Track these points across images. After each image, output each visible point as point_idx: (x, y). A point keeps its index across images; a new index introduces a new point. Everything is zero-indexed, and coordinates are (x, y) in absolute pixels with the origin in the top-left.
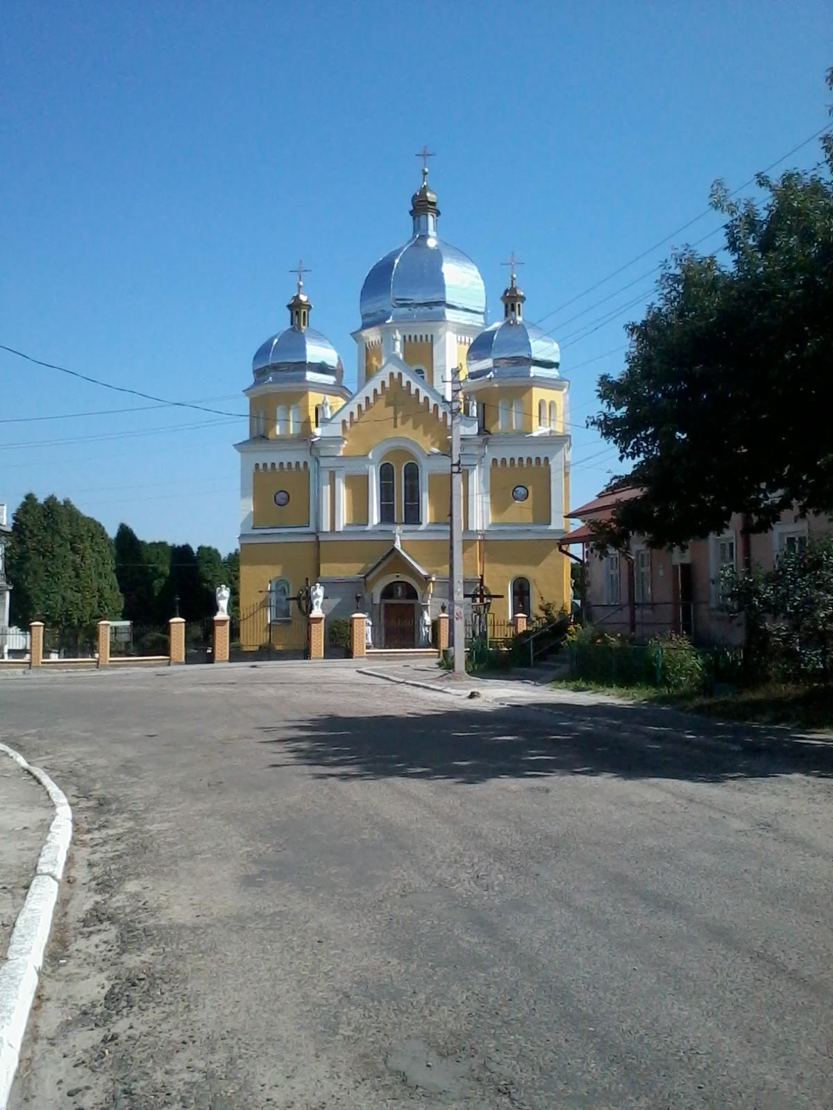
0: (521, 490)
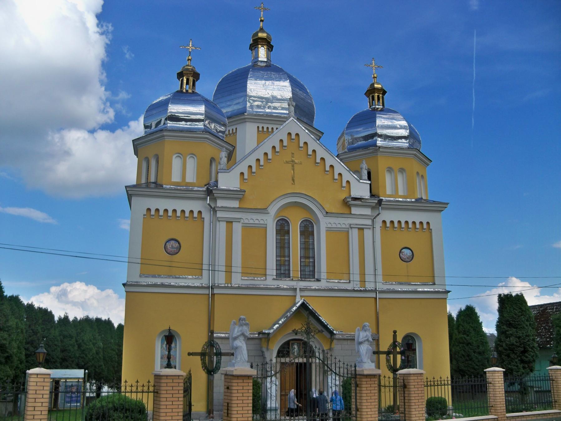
0: (407, 252)
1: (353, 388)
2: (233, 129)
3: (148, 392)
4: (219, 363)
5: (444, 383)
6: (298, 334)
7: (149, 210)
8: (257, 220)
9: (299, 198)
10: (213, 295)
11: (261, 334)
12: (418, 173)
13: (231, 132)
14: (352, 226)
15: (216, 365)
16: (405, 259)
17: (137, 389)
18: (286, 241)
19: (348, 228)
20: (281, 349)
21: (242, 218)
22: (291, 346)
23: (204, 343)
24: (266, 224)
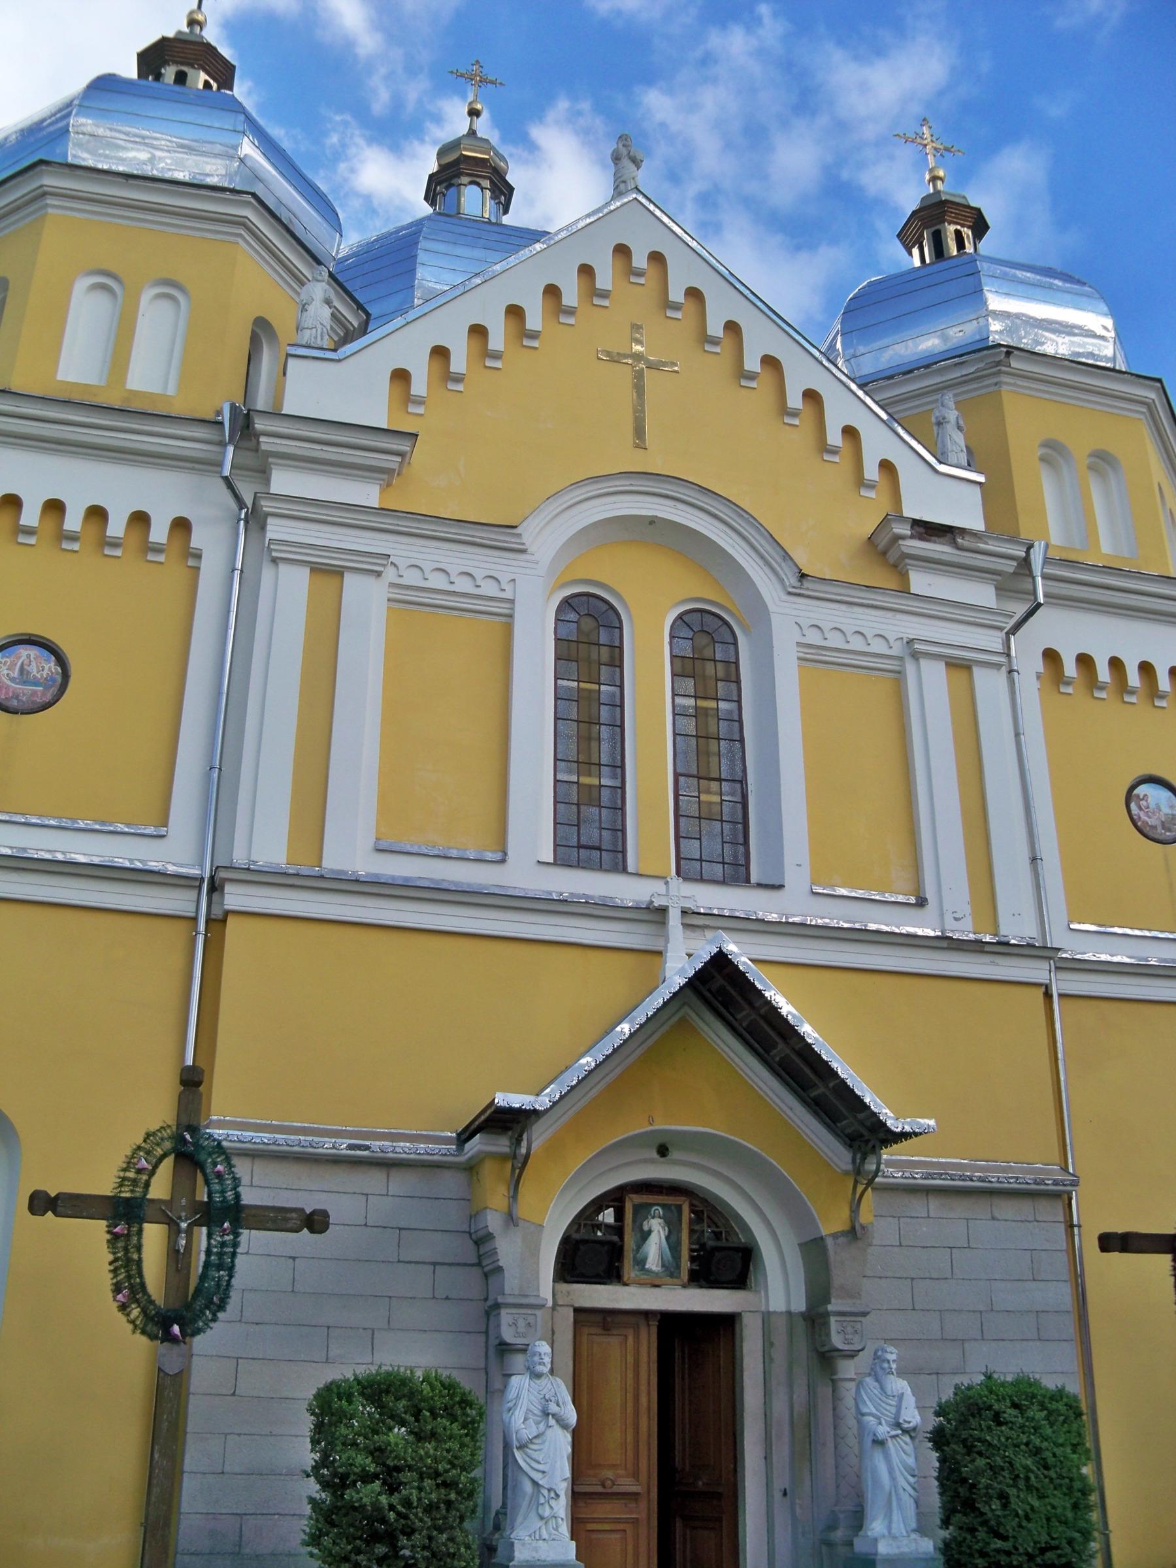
4: (220, 1267)
6: (674, 1154)
8: (466, 579)
10: (218, 922)
15: (203, 1277)
16: (1154, 827)
19: (901, 659)
20: (576, 1236)
22: (634, 1221)
23: (139, 1141)
24: (512, 601)
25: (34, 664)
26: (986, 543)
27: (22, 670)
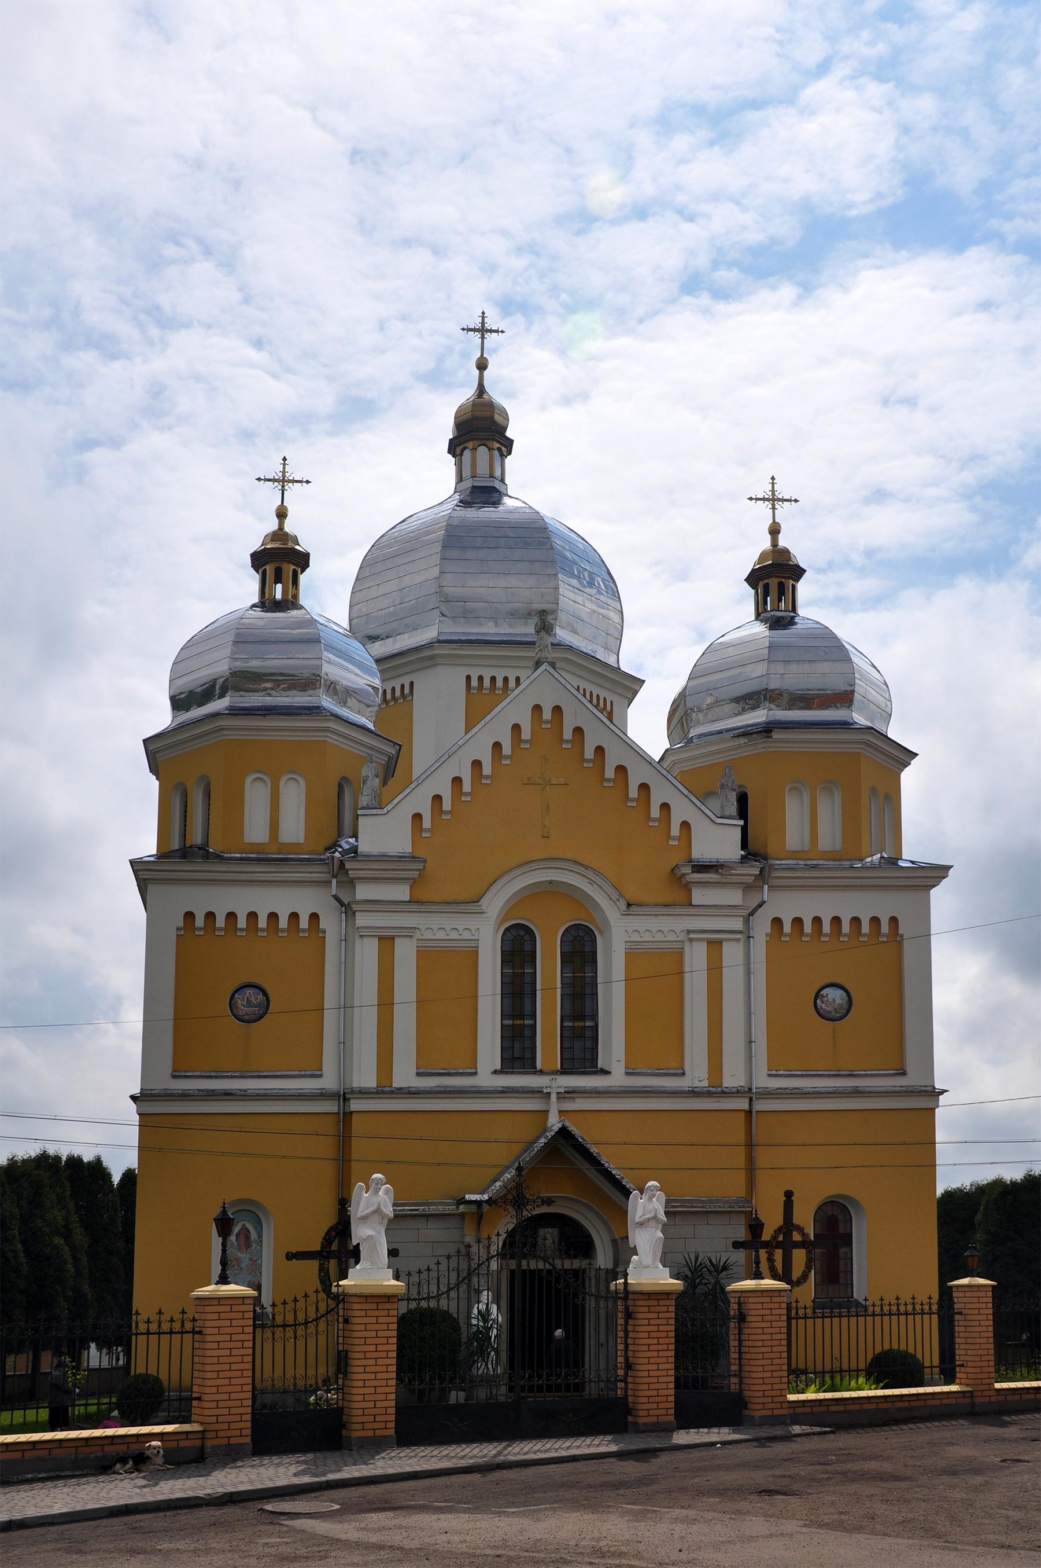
0: (835, 996)
1: (621, 1321)
2: (403, 686)
3: (182, 1333)
5: (874, 1311)
7: (189, 916)
8: (455, 932)
9: (560, 871)
10: (348, 1115)
11: (462, 1203)
12: (874, 790)
13: (398, 693)
14: (692, 936)
16: (830, 1012)
17: (160, 1326)
18: (527, 980)
21: (417, 926)
24: (478, 940)
25: (253, 997)
26: (736, 870)
27: (248, 1001)
